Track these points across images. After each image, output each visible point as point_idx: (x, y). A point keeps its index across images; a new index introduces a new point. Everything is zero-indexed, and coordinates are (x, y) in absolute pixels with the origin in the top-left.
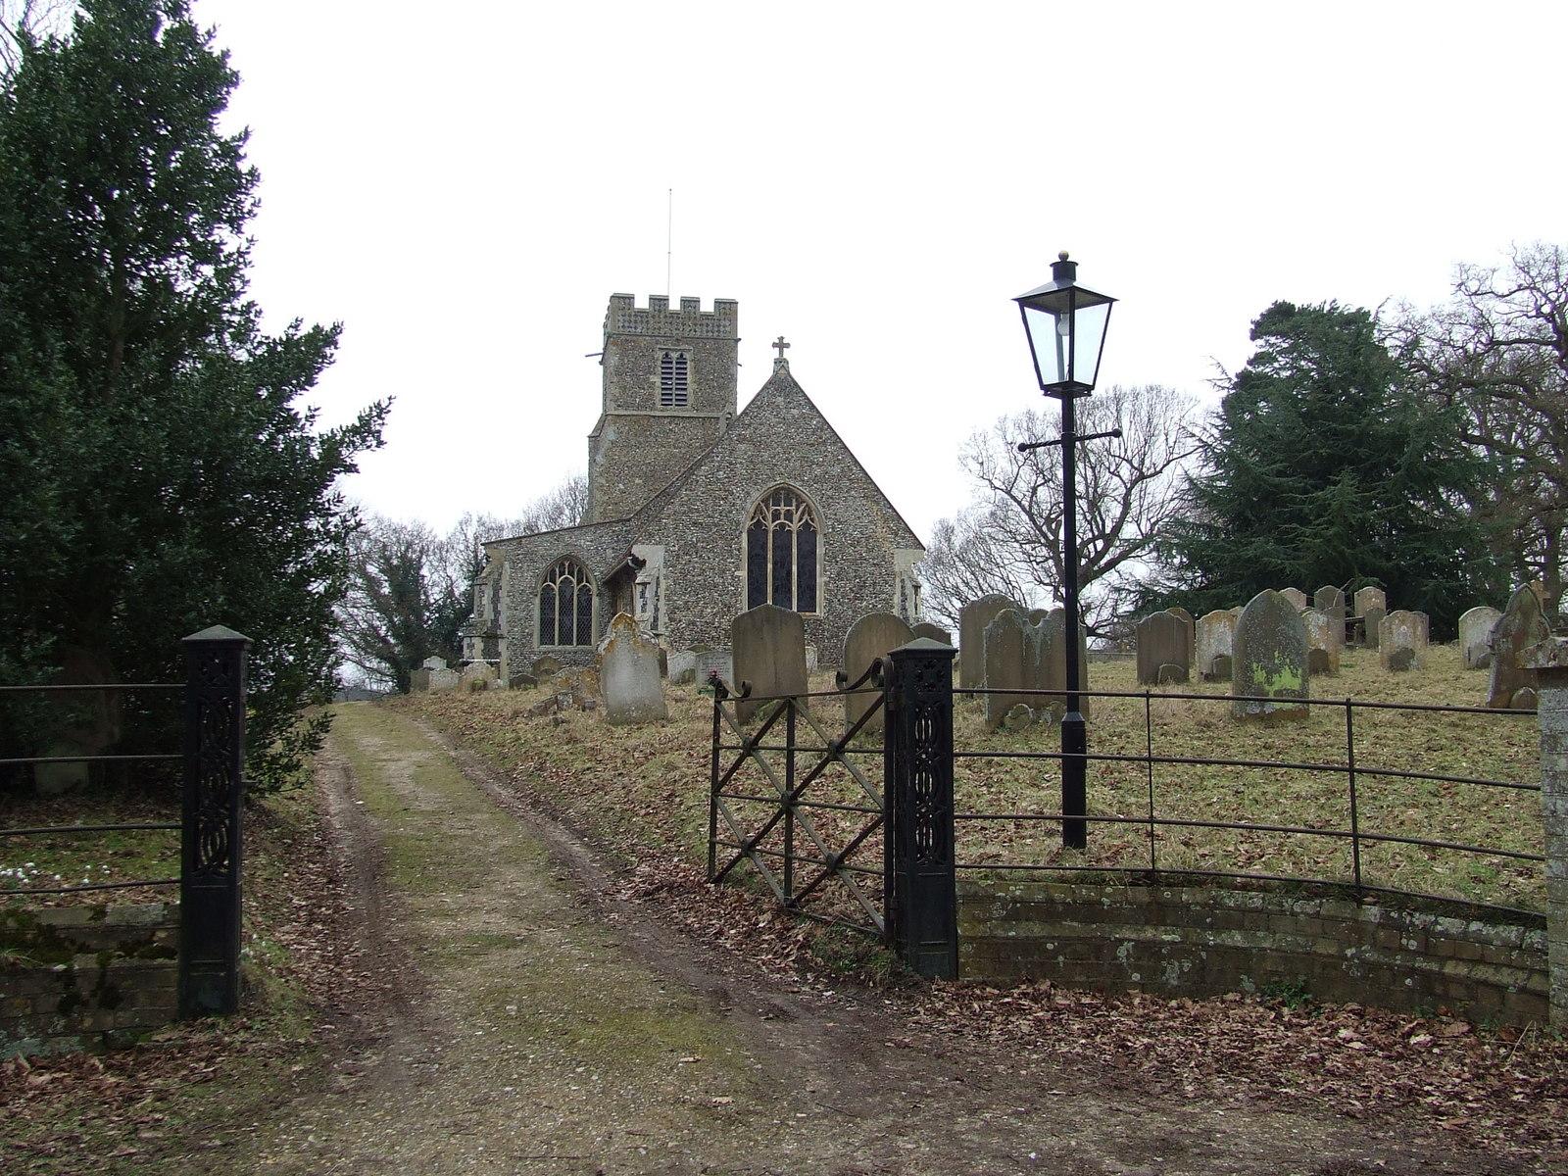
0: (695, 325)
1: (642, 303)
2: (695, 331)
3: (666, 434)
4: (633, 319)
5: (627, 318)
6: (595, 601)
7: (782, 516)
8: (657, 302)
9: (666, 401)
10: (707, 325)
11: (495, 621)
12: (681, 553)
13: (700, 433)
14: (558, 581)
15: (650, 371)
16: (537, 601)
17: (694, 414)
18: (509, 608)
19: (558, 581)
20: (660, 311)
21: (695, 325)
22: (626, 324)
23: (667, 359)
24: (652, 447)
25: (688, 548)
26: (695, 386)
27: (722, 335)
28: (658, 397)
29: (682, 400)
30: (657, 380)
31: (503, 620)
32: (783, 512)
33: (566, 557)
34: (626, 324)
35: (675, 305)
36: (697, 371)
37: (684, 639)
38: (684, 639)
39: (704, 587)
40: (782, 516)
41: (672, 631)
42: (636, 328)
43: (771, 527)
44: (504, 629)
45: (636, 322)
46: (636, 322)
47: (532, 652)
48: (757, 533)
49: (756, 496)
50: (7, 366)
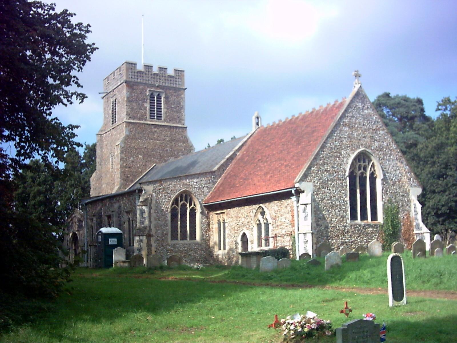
0: (165, 80)
1: (140, 67)
2: (165, 83)
3: (153, 133)
4: (136, 74)
5: (133, 73)
6: (198, 216)
7: (362, 169)
8: (147, 68)
9: (152, 117)
10: (171, 81)
11: (150, 227)
12: (321, 187)
13: (169, 133)
14: (180, 204)
15: (144, 101)
16: (170, 214)
17: (166, 124)
18: (155, 219)
19: (180, 204)
20: (149, 72)
21: (165, 80)
22: (133, 77)
23: (152, 97)
24: (147, 140)
25: (324, 184)
26: (165, 110)
27: (177, 86)
28: (148, 115)
29: (159, 117)
30: (147, 105)
31: (152, 227)
32: (363, 166)
33: (185, 191)
34: (133, 77)
35: (155, 70)
36: (167, 102)
37: (323, 236)
38: (323, 236)
39: (332, 207)
40: (362, 169)
41: (318, 232)
42: (138, 79)
43: (359, 173)
44: (153, 232)
45: (137, 76)
46: (137, 76)
47: (168, 244)
48: (352, 176)
49: (353, 156)
50: (49, 37)
